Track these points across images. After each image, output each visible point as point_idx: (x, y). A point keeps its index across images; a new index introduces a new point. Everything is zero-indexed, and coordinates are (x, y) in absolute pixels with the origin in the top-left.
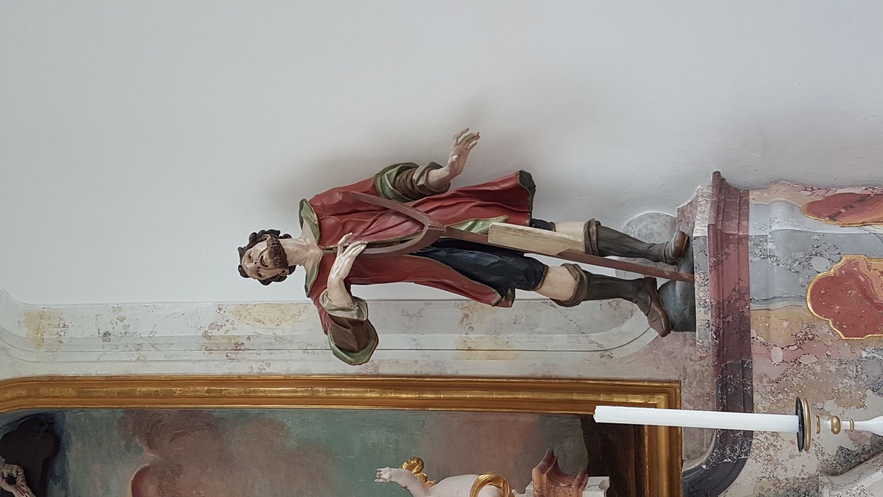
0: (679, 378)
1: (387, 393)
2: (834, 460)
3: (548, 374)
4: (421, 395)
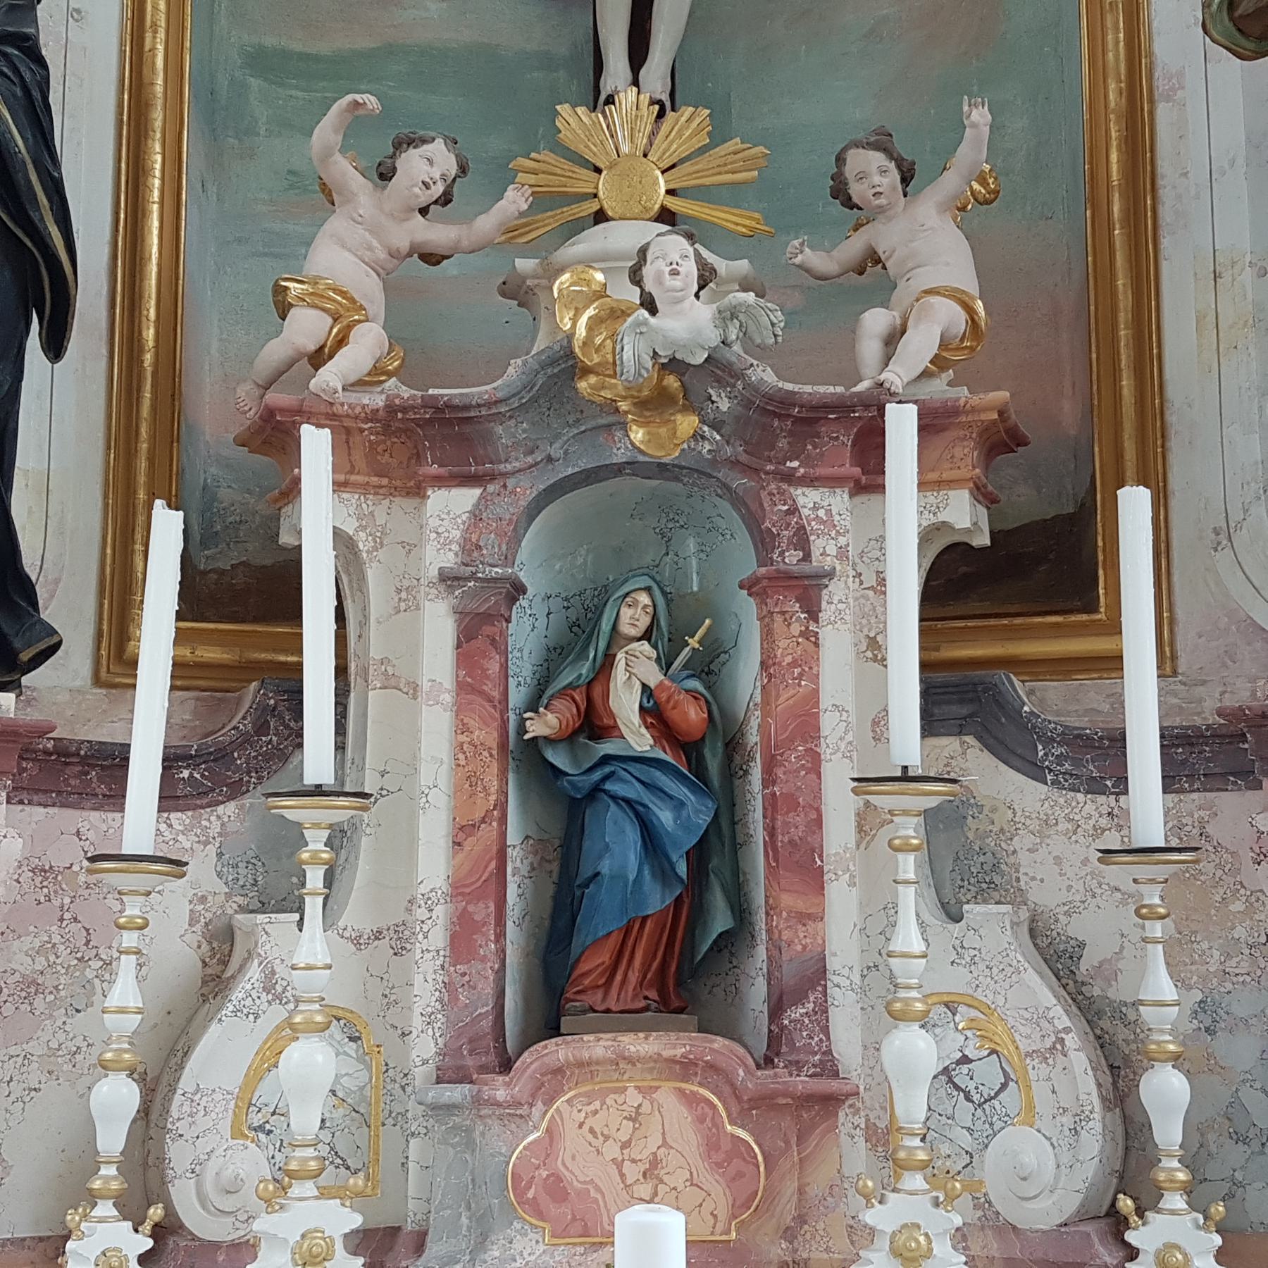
0: (1182, 674)
1: (1117, 122)
2: (1058, 934)
3: (1173, 432)
4: (1116, 189)
